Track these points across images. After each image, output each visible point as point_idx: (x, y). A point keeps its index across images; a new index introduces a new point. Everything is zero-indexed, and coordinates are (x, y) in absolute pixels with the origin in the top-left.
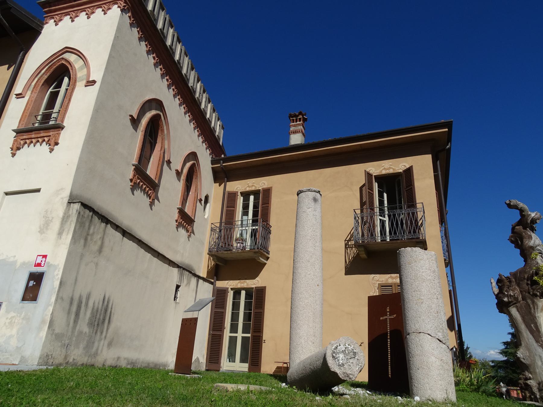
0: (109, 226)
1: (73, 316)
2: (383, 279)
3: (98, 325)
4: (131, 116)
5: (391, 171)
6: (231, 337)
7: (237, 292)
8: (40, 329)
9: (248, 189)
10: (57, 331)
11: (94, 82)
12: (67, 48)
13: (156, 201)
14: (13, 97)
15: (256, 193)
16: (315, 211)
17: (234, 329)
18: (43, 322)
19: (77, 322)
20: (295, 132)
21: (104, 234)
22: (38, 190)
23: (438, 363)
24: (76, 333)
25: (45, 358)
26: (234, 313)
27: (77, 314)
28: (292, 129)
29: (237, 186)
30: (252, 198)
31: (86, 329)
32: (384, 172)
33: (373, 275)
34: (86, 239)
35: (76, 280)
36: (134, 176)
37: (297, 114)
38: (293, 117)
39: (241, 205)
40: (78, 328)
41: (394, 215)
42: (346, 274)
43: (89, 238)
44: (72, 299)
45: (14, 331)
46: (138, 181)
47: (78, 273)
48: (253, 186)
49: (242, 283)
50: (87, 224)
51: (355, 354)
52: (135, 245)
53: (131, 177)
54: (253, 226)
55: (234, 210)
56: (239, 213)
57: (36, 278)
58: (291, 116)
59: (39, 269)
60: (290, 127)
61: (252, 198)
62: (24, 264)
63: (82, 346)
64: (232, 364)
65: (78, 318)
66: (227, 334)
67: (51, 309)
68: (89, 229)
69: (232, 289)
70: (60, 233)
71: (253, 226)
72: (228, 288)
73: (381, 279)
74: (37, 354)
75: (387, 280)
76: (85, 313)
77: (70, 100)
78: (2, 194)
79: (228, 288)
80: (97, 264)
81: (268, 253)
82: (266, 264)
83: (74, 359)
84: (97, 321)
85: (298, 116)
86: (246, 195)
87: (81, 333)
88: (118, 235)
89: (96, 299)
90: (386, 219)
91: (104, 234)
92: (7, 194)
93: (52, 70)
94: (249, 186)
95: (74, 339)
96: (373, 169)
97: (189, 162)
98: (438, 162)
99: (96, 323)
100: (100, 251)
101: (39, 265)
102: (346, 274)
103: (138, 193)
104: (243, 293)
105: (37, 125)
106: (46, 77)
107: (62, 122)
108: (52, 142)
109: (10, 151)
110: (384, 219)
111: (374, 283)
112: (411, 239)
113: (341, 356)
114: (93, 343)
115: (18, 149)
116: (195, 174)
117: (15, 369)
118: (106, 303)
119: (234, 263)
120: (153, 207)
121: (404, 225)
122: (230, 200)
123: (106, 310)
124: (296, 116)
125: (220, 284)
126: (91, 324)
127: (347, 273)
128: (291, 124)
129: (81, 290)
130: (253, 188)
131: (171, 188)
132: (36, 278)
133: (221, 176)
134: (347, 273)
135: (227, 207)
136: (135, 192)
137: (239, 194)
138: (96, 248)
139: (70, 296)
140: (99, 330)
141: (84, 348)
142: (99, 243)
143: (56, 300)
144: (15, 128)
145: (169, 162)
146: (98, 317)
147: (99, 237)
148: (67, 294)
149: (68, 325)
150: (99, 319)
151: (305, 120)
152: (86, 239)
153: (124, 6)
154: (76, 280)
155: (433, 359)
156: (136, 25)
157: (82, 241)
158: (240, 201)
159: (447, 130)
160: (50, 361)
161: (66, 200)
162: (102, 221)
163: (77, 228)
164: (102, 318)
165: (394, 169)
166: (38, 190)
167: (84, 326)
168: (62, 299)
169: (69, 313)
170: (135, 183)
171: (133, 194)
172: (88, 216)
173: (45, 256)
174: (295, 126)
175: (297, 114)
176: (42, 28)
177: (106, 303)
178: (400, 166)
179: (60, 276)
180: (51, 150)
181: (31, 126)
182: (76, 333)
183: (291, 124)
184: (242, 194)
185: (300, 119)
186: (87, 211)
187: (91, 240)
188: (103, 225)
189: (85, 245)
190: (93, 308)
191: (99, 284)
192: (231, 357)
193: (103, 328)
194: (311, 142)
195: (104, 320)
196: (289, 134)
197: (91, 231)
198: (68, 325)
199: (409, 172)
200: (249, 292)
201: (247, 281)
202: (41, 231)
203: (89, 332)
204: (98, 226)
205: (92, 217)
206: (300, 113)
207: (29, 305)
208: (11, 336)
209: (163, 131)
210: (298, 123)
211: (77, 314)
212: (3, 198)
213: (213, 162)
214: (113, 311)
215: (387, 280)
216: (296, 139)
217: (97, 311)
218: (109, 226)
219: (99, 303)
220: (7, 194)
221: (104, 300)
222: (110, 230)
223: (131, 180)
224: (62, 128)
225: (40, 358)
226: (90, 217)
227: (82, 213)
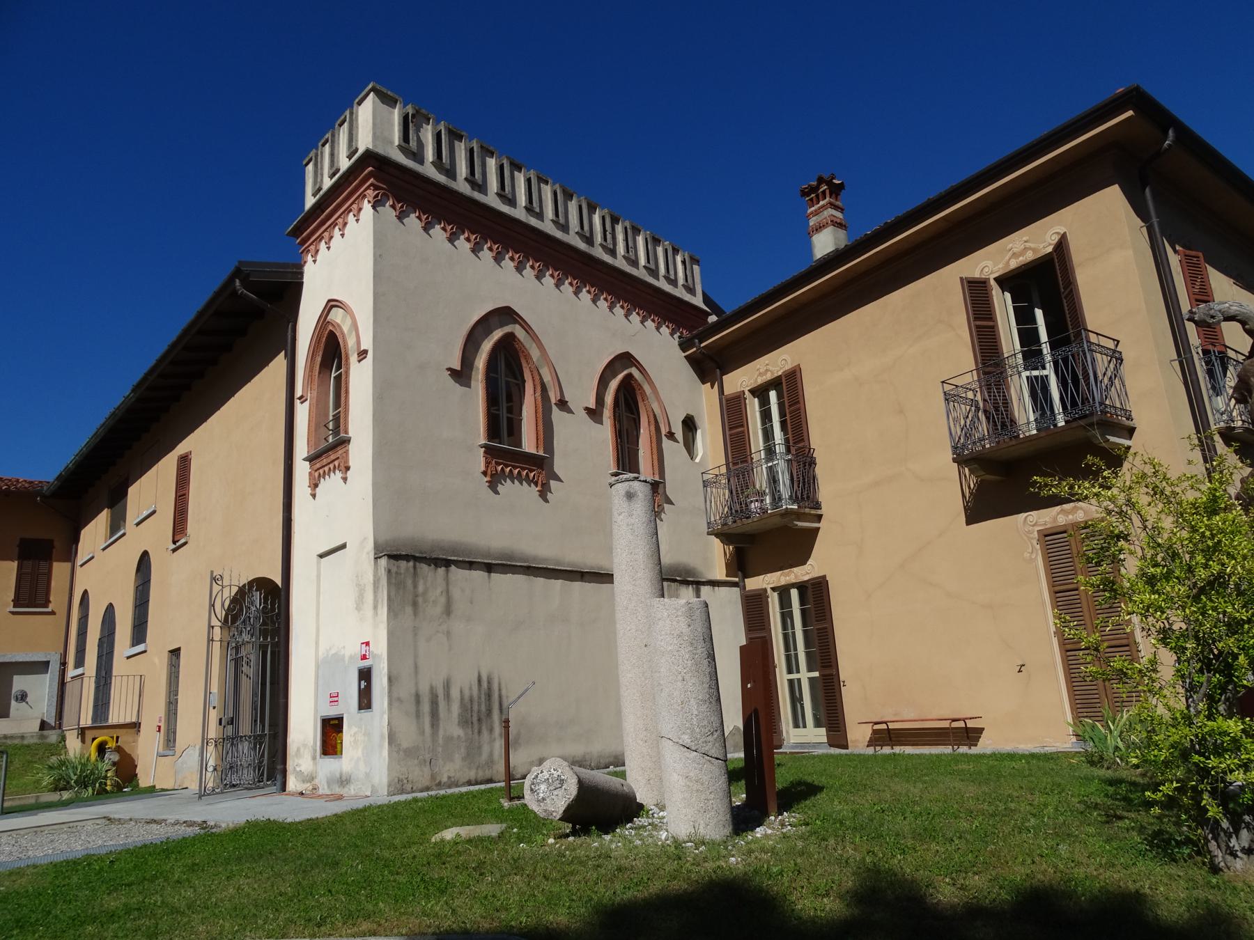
0: (453, 567)
1: (427, 720)
2: (1047, 519)
3: (479, 720)
4: (449, 369)
5: (1030, 256)
6: (791, 682)
7: (783, 592)
8: (381, 746)
9: (760, 381)
10: (405, 745)
11: (365, 352)
12: (329, 301)
13: (552, 482)
14: (297, 402)
15: (775, 383)
16: (631, 515)
17: (792, 667)
18: (382, 736)
19: (438, 726)
20: (819, 228)
21: (448, 584)
22: (343, 546)
23: (682, 782)
24: (441, 741)
25: (398, 785)
26: (786, 636)
27: (434, 714)
28: (813, 222)
29: (741, 380)
30: (773, 395)
31: (457, 732)
32: (1014, 264)
33: (1024, 515)
34: (415, 604)
35: (416, 667)
36: (488, 464)
37: (815, 183)
38: (811, 193)
39: (758, 415)
40: (441, 733)
41: (1065, 360)
42: (968, 523)
43: (420, 600)
44: (418, 698)
45: (360, 753)
46: (499, 468)
47: (416, 656)
48: (767, 370)
49: (788, 575)
50: (409, 582)
51: (562, 782)
52: (520, 579)
53: (483, 468)
54: (767, 462)
55: (976, 319)
56: (756, 433)
57: (365, 675)
58: (804, 193)
59: (366, 663)
60: (808, 218)
61: (773, 395)
62: (351, 657)
63: (458, 757)
64: (801, 731)
65: (438, 719)
66: (782, 677)
67: (386, 717)
68: (415, 586)
69: (774, 589)
70: (375, 607)
71: (767, 462)
72: (765, 590)
73: (1041, 521)
74: (385, 781)
75: (1055, 519)
76: (449, 710)
77: (347, 392)
78: (315, 558)
79: (765, 590)
80: (448, 634)
81: (818, 506)
82: (818, 529)
83: (449, 778)
84: (475, 715)
85: (818, 187)
86: (760, 392)
87: (449, 739)
88: (479, 575)
89: (464, 681)
90: (1049, 371)
91: (448, 584)
92: (321, 556)
93: (322, 345)
94: (761, 374)
95: (440, 749)
96: (989, 263)
97: (615, 376)
98: (1147, 190)
99: (475, 719)
100: (448, 611)
101: (364, 657)
102: (968, 523)
103: (507, 487)
104: (794, 593)
105: (331, 439)
106: (319, 359)
107: (346, 432)
108: (342, 468)
109: (309, 491)
110: (1045, 373)
111: (1029, 532)
112: (1080, 418)
113: (543, 787)
114: (480, 747)
115: (316, 486)
116: (638, 392)
117: (344, 809)
118: (485, 685)
119: (767, 538)
120: (549, 496)
121: (1070, 384)
122: (733, 410)
123: (489, 696)
124: (814, 189)
125: (753, 583)
126: (465, 722)
127: (970, 520)
128: (810, 211)
129: (431, 677)
130: (769, 377)
131: (583, 444)
132: (365, 675)
133: (709, 366)
134: (970, 520)
135: (730, 429)
136: (500, 488)
137: (747, 394)
138: (439, 609)
139: (413, 691)
140: (484, 728)
141: (464, 759)
142: (443, 600)
143: (390, 704)
144: (305, 455)
145: (563, 404)
146: (476, 708)
147: (439, 591)
148: (406, 690)
149: (422, 733)
150: (479, 711)
151: (836, 190)
152: (415, 604)
153: (376, 196)
154: (416, 667)
155: (675, 777)
156: (410, 209)
157: (409, 610)
158: (753, 406)
159: (1130, 113)
160: (409, 787)
161: (372, 556)
162: (437, 566)
163: (393, 593)
164: (483, 708)
165: (1034, 250)
166: (343, 546)
167: (451, 726)
168: (399, 699)
169: (418, 715)
170: (492, 476)
171: (497, 493)
172: (407, 569)
173: (367, 644)
174: (816, 213)
175: (815, 183)
176: (302, 274)
177: (485, 685)
178: (1048, 237)
179: (386, 670)
180: (345, 479)
181: (323, 445)
182: (441, 741)
183: (810, 211)
184: (753, 392)
185: (824, 192)
186: (403, 564)
187: (425, 601)
188: (441, 571)
189: (415, 614)
190: (462, 699)
191: (460, 660)
192: (798, 722)
193: (492, 722)
194: (859, 236)
195: (489, 712)
196: (810, 235)
197: (421, 588)
198: (422, 733)
199: (1062, 246)
200: (802, 587)
201: (795, 569)
202: (358, 608)
203: (466, 734)
204: (432, 578)
205: (415, 567)
206: (821, 180)
207: (365, 714)
208: (358, 759)
209: (528, 357)
210: (822, 203)
211: (434, 714)
212: (318, 563)
213: (684, 346)
214: (504, 692)
215: (1055, 519)
216: (825, 243)
217: (471, 700)
218: (453, 567)
219: (471, 689)
220: (321, 556)
221: (479, 681)
222: (457, 573)
223: (485, 473)
224: (348, 441)
225: (389, 786)
226: (412, 570)
227: (394, 570)
